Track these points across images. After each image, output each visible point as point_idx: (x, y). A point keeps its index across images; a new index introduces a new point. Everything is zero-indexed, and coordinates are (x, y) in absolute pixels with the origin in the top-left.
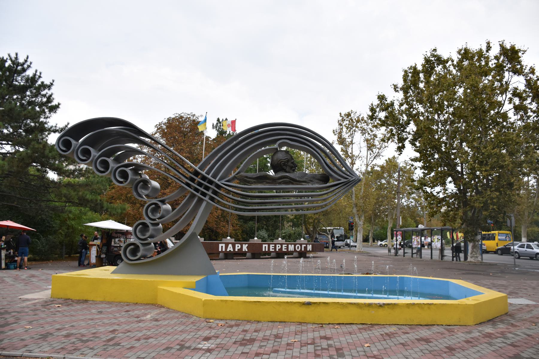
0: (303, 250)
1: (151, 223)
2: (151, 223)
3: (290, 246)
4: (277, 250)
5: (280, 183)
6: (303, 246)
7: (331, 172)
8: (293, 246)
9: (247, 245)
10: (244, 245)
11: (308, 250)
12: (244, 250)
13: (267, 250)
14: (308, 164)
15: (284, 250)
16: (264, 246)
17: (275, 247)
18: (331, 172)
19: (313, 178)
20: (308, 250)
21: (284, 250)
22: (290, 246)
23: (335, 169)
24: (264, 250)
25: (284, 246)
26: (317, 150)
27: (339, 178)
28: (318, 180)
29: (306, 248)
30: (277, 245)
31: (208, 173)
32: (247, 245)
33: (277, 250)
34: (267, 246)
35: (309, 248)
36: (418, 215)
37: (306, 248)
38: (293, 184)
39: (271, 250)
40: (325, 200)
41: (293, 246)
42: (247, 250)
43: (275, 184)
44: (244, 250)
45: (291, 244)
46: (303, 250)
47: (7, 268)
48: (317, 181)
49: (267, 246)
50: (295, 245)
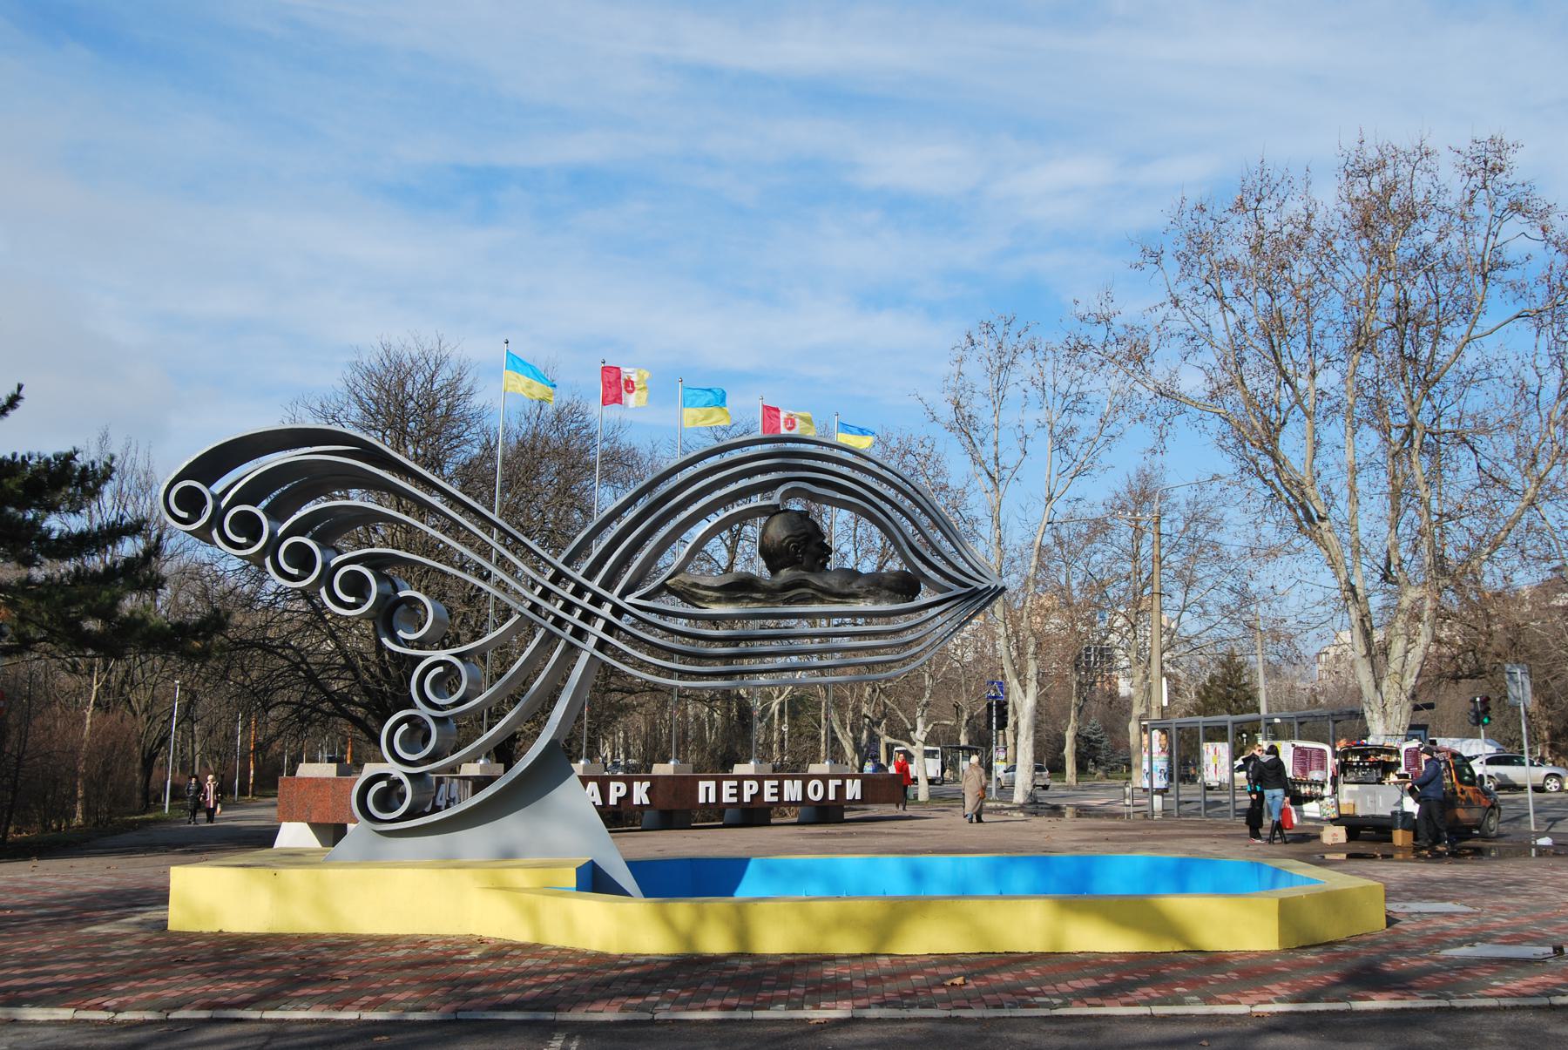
0: (832, 796)
1: (433, 718)
2: (433, 718)
3: (787, 783)
4: (747, 799)
5: (788, 602)
6: (832, 784)
7: (924, 569)
8: (798, 783)
9: (647, 784)
10: (636, 784)
11: (849, 797)
12: (636, 801)
13: (712, 799)
14: (851, 541)
15: (767, 798)
16: (702, 785)
17: (740, 788)
18: (924, 569)
19: (878, 585)
20: (849, 797)
21: (767, 798)
22: (787, 783)
23: (936, 561)
24: (702, 799)
25: (767, 784)
26: (882, 504)
27: (947, 583)
28: (890, 589)
29: (840, 790)
30: (746, 784)
31: (590, 575)
32: (647, 784)
33: (747, 799)
34: (712, 784)
35: (853, 790)
36: (645, 744)
37: (840, 790)
38: (822, 601)
39: (726, 799)
40: (908, 644)
41: (798, 783)
42: (646, 801)
43: (774, 604)
44: (636, 801)
45: (793, 778)
46: (832, 796)
47: (1271, 840)
48: (886, 593)
49: (712, 784)
50: (806, 780)
